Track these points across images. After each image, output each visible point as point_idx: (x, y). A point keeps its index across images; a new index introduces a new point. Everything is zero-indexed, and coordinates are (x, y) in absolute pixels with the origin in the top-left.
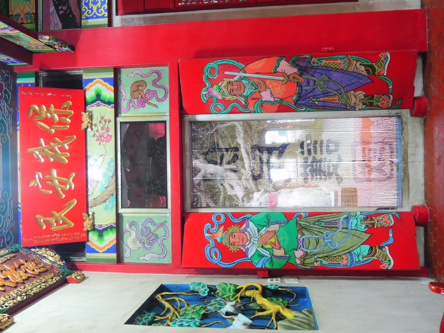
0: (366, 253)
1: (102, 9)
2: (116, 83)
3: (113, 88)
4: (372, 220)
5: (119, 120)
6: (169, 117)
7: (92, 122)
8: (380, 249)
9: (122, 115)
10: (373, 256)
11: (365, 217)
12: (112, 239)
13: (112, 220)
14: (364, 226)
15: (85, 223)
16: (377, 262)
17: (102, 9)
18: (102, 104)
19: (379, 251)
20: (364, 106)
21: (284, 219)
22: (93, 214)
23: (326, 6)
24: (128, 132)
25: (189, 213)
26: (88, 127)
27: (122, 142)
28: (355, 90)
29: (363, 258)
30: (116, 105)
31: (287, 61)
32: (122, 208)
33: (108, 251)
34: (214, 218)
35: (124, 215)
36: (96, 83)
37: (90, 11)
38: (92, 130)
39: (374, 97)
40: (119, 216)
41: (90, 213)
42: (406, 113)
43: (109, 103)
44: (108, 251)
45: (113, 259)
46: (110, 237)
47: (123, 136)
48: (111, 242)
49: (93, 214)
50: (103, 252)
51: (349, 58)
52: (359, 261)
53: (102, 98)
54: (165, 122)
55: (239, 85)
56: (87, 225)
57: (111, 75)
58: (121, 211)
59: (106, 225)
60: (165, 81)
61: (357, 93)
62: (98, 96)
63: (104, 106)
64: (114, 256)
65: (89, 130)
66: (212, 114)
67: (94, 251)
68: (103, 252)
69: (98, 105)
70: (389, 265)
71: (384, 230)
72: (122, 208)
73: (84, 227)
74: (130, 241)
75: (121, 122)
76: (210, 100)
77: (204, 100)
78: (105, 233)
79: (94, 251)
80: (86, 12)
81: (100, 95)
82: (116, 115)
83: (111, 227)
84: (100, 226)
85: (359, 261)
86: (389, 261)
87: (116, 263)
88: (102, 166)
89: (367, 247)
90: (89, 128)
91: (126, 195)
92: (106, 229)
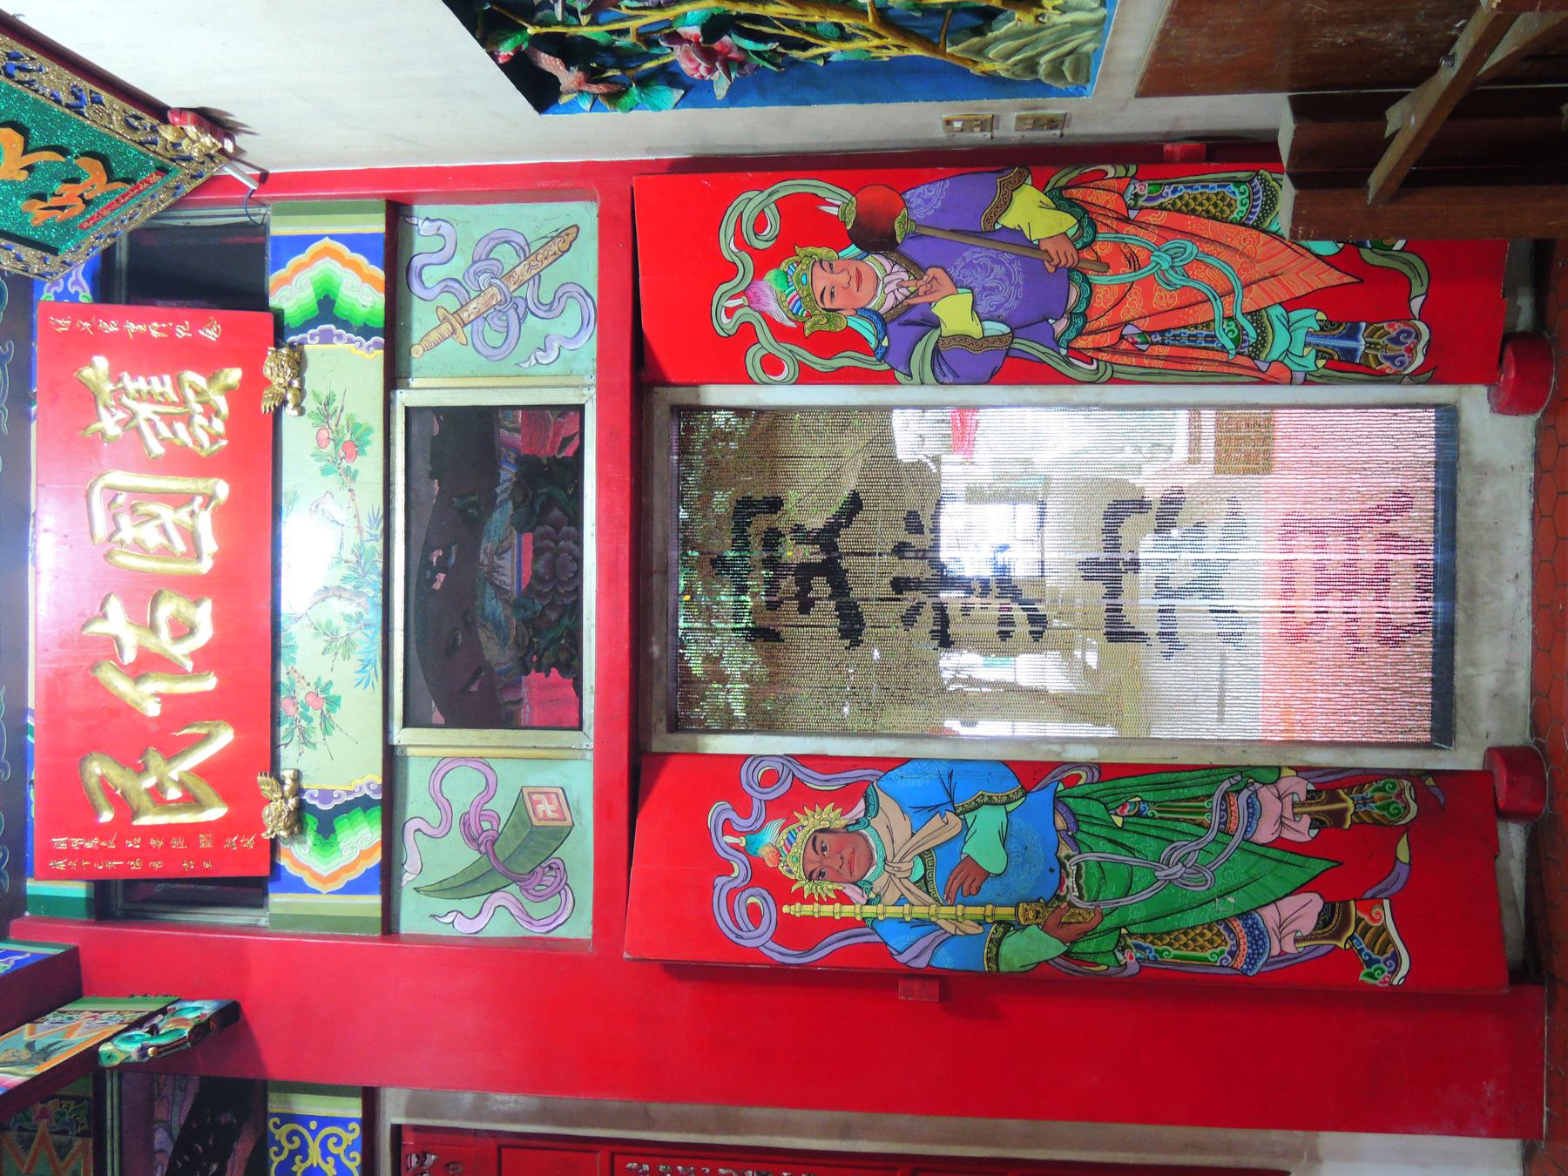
0: (1307, 923)
1: (287, 1147)
2: (394, 257)
3: (380, 274)
4: (1335, 798)
5: (403, 398)
6: (593, 391)
7: (302, 383)
8: (1364, 912)
9: (414, 383)
10: (1337, 935)
11: (1311, 787)
12: (366, 845)
13: (369, 777)
14: (1307, 820)
15: (266, 811)
16: (1349, 961)
17: (287, 1147)
18: (340, 337)
19: (1359, 921)
20: (1321, 363)
21: (1012, 785)
22: (298, 776)
23: (1084, 1148)
24: (437, 444)
25: (665, 756)
26: (285, 402)
27: (413, 580)
28: (1290, 305)
29: (1296, 941)
30: (392, 335)
31: (1040, 185)
32: (405, 725)
33: (352, 888)
34: (748, 778)
35: (410, 751)
36: (334, 877)
37: (334, 1150)
38: (302, 412)
39: (1358, 329)
40: (392, 758)
41: (287, 774)
42: (1474, 401)
43: (366, 332)
44: (352, 888)
45: (371, 918)
46: (360, 838)
47: (420, 533)
48: (365, 854)
49: (298, 776)
50: (319, 237)
51: (1264, 181)
52: (1282, 953)
53: (341, 309)
54: (580, 409)
55: (853, 273)
56: (274, 815)
57: (376, 225)
58: (400, 736)
59: (349, 793)
60: (583, 264)
61: (1294, 315)
62: (326, 309)
63: (350, 341)
64: (372, 903)
65: (289, 413)
66: (751, 382)
67: (298, 886)
68: (319, 237)
69: (326, 338)
70: (1394, 972)
71: (1379, 835)
72: (405, 725)
73: (265, 829)
74: (433, 855)
75: (407, 409)
76: (746, 334)
77: (726, 325)
78: (341, 824)
79: (298, 886)
80: (344, 1145)
81: (333, 302)
82: (394, 376)
83: (364, 803)
84: (326, 795)
85: (1282, 953)
86: (1396, 957)
87: (378, 934)
88: (336, 544)
89: (1314, 903)
90: (290, 405)
91: (423, 466)
92: (346, 808)
